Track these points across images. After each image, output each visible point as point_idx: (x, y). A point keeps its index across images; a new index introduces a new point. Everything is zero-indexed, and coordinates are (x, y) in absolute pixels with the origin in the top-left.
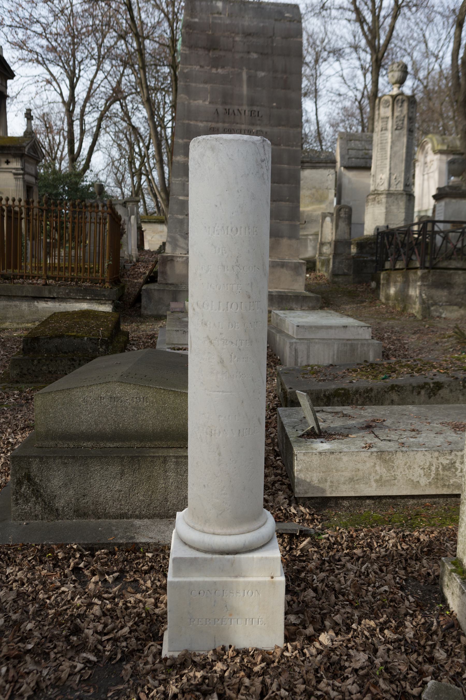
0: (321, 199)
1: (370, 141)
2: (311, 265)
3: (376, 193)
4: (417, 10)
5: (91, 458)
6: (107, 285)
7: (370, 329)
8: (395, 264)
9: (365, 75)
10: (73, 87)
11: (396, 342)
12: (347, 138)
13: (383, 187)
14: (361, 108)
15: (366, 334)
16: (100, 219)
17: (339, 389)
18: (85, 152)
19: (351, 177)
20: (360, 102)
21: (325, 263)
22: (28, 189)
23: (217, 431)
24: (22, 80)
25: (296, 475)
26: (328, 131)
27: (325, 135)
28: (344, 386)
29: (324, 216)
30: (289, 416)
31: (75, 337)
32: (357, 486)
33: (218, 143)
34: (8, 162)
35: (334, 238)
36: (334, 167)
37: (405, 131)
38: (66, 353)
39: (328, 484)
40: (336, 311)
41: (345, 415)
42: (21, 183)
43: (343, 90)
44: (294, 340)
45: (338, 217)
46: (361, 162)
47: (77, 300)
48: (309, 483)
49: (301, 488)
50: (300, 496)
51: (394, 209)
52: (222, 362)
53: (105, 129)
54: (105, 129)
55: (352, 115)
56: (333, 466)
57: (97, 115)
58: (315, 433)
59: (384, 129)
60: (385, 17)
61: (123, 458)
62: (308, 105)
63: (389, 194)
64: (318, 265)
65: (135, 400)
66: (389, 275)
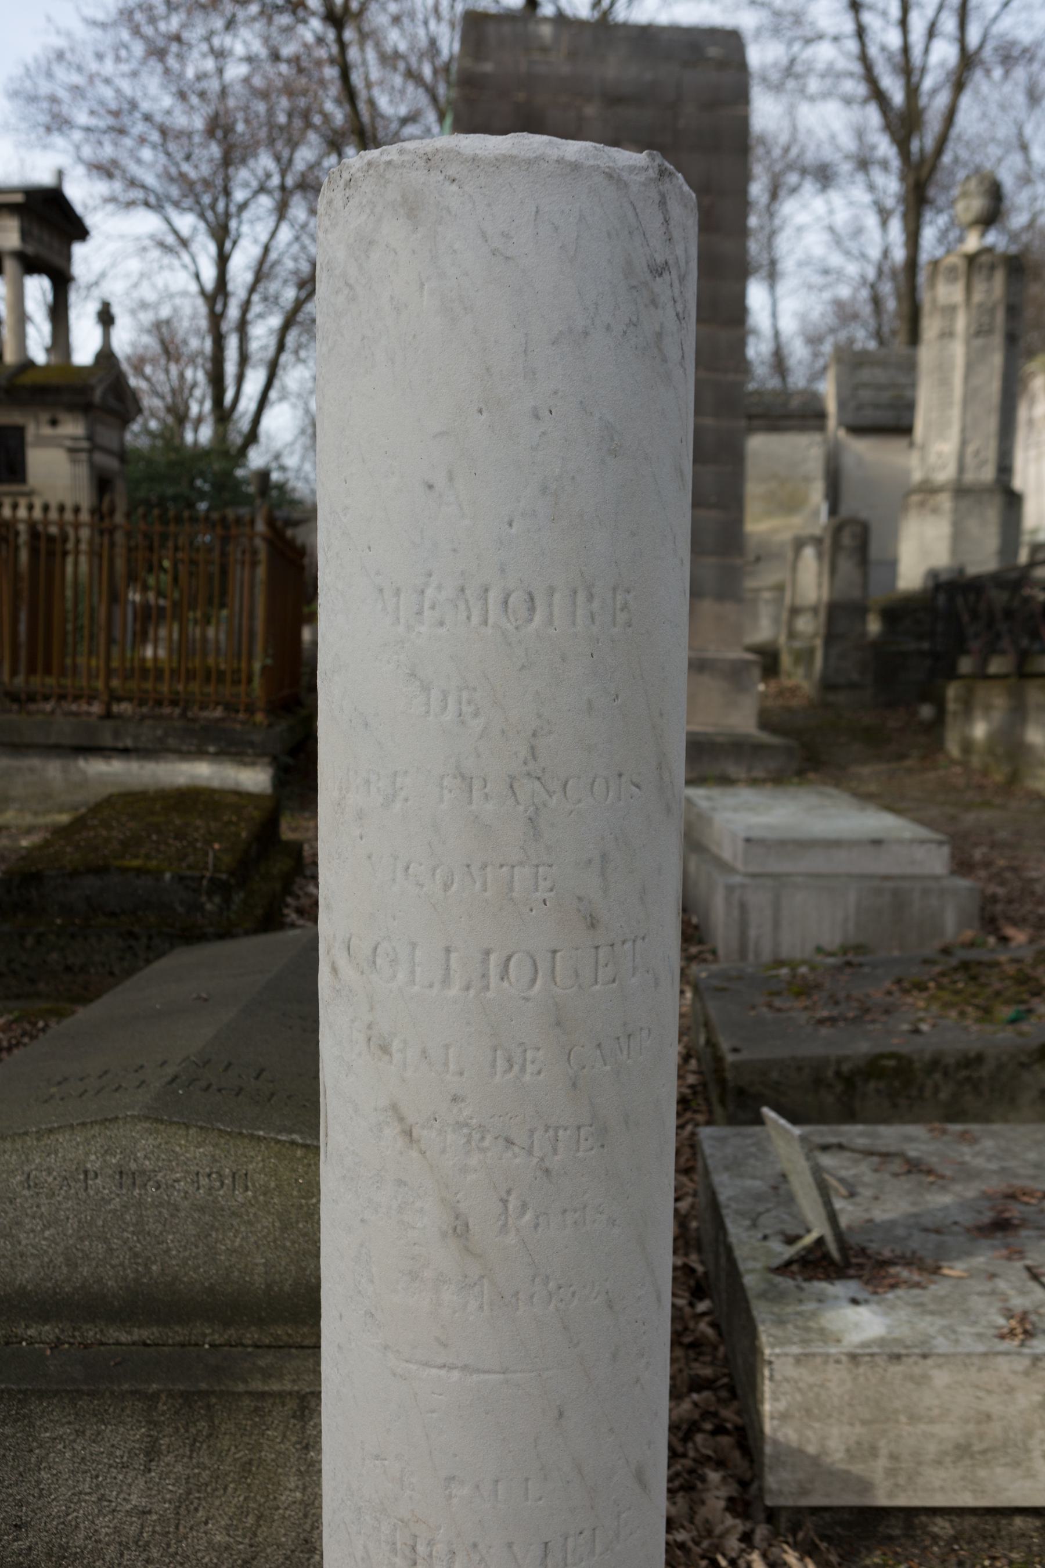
0: (791, 505)
1: (910, 367)
2: (769, 661)
3: (929, 488)
4: (1007, 74)
5: (41, 1395)
6: (259, 717)
7: (946, 850)
8: (985, 662)
9: (884, 223)
10: (223, 260)
11: (1008, 875)
12: (850, 360)
13: (946, 474)
14: (876, 301)
15: (934, 860)
16: (244, 552)
17: (882, 1056)
18: (247, 404)
19: (863, 451)
20: (873, 286)
21: (804, 657)
22: (102, 483)
23: (440, 1548)
24: (112, 247)
25: (768, 1427)
26: (798, 352)
27: (792, 362)
28: (895, 1044)
29: (799, 544)
30: (734, 1166)
31: (139, 871)
32: (982, 1473)
33: (436, 177)
34: (54, 423)
35: (825, 596)
36: (821, 428)
37: (997, 340)
38: (113, 914)
39: (882, 1462)
40: (837, 785)
41: (914, 1167)
42: (83, 471)
43: (836, 260)
44: (737, 879)
45: (836, 546)
46: (885, 417)
47: (185, 755)
48: (815, 1461)
49: (785, 1475)
50: (782, 1502)
51: (973, 526)
52: (460, 1230)
53: (296, 352)
54: (296, 352)
55: (855, 317)
56: (897, 1404)
57: (275, 321)
58: (826, 1256)
59: (947, 334)
60: (934, 92)
61: (155, 1397)
62: (756, 295)
63: (961, 491)
64: (786, 661)
65: (204, 1181)
66: (970, 691)
